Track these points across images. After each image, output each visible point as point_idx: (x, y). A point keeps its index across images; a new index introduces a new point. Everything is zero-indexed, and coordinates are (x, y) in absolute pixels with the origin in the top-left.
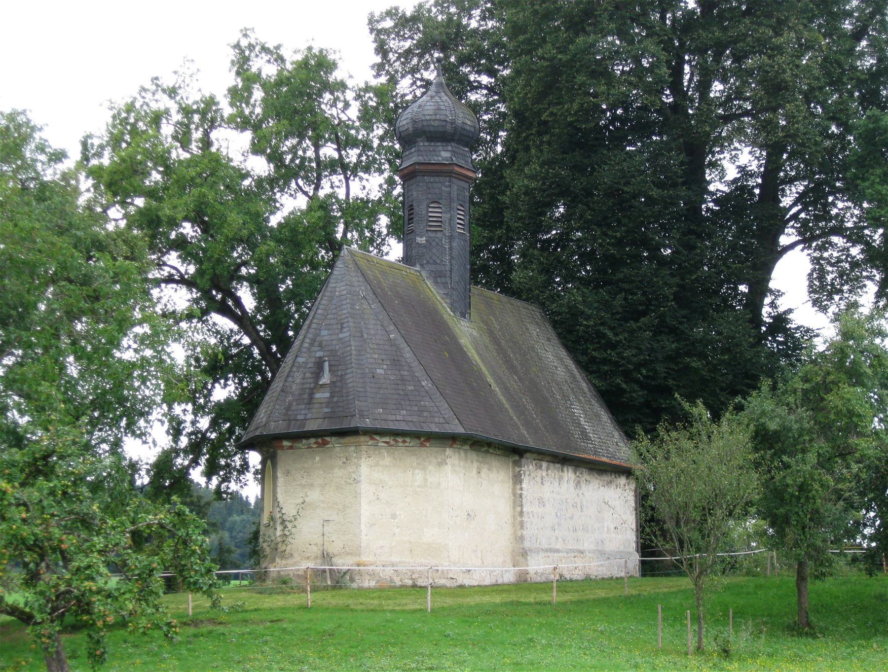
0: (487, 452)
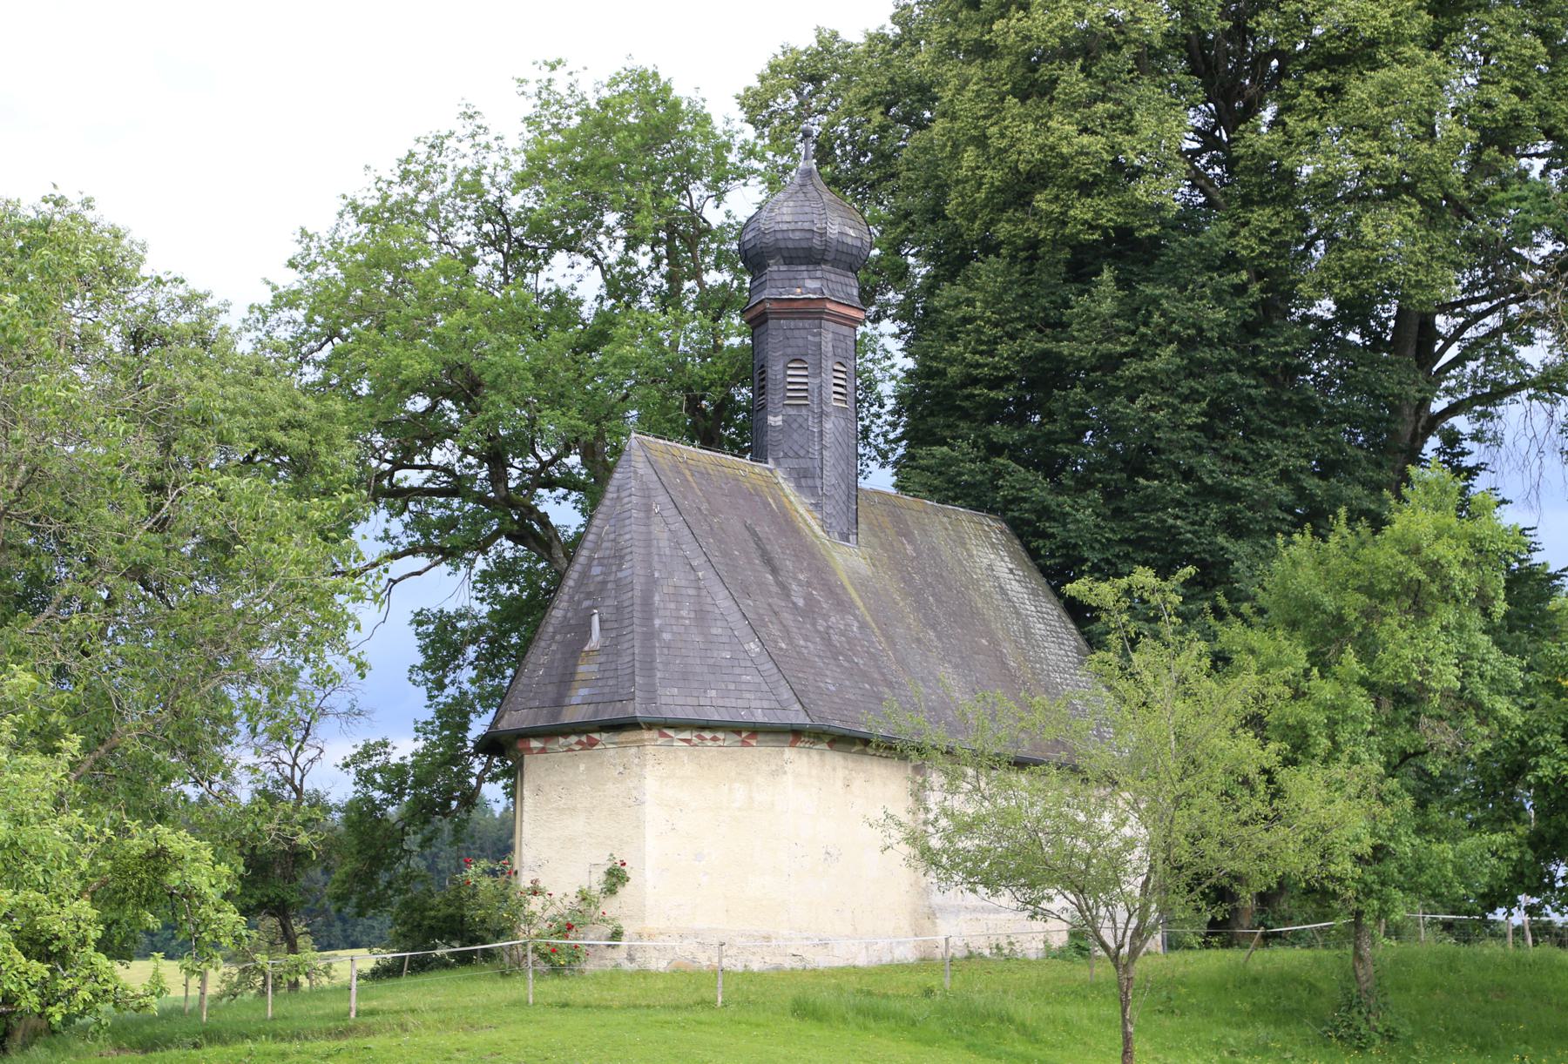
0: (864, 753)
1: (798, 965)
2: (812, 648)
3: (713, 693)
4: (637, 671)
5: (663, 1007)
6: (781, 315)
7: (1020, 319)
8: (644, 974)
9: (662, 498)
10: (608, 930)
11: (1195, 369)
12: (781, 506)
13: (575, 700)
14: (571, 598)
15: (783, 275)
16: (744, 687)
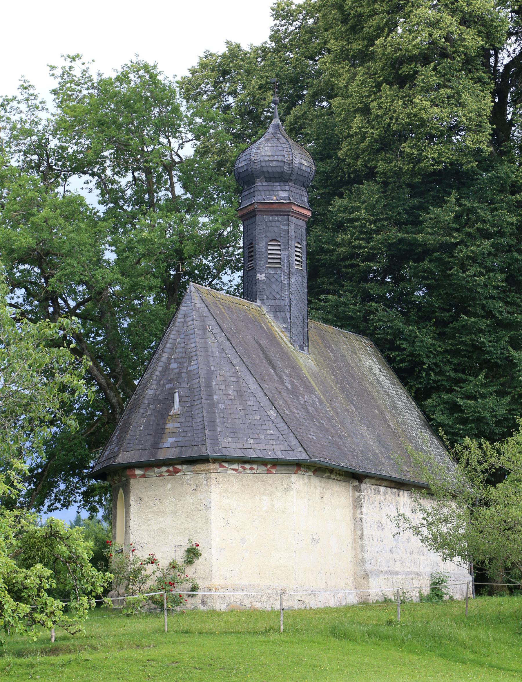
1: (302, 607)
2: (300, 414)
3: (252, 441)
4: (206, 427)
5: (221, 633)
6: (264, 213)
7: (385, 219)
8: (212, 612)
9: (212, 322)
10: (189, 586)
11: (498, 249)
12: (268, 329)
13: (166, 445)
14: (158, 382)
15: (265, 188)
16: (269, 437)
